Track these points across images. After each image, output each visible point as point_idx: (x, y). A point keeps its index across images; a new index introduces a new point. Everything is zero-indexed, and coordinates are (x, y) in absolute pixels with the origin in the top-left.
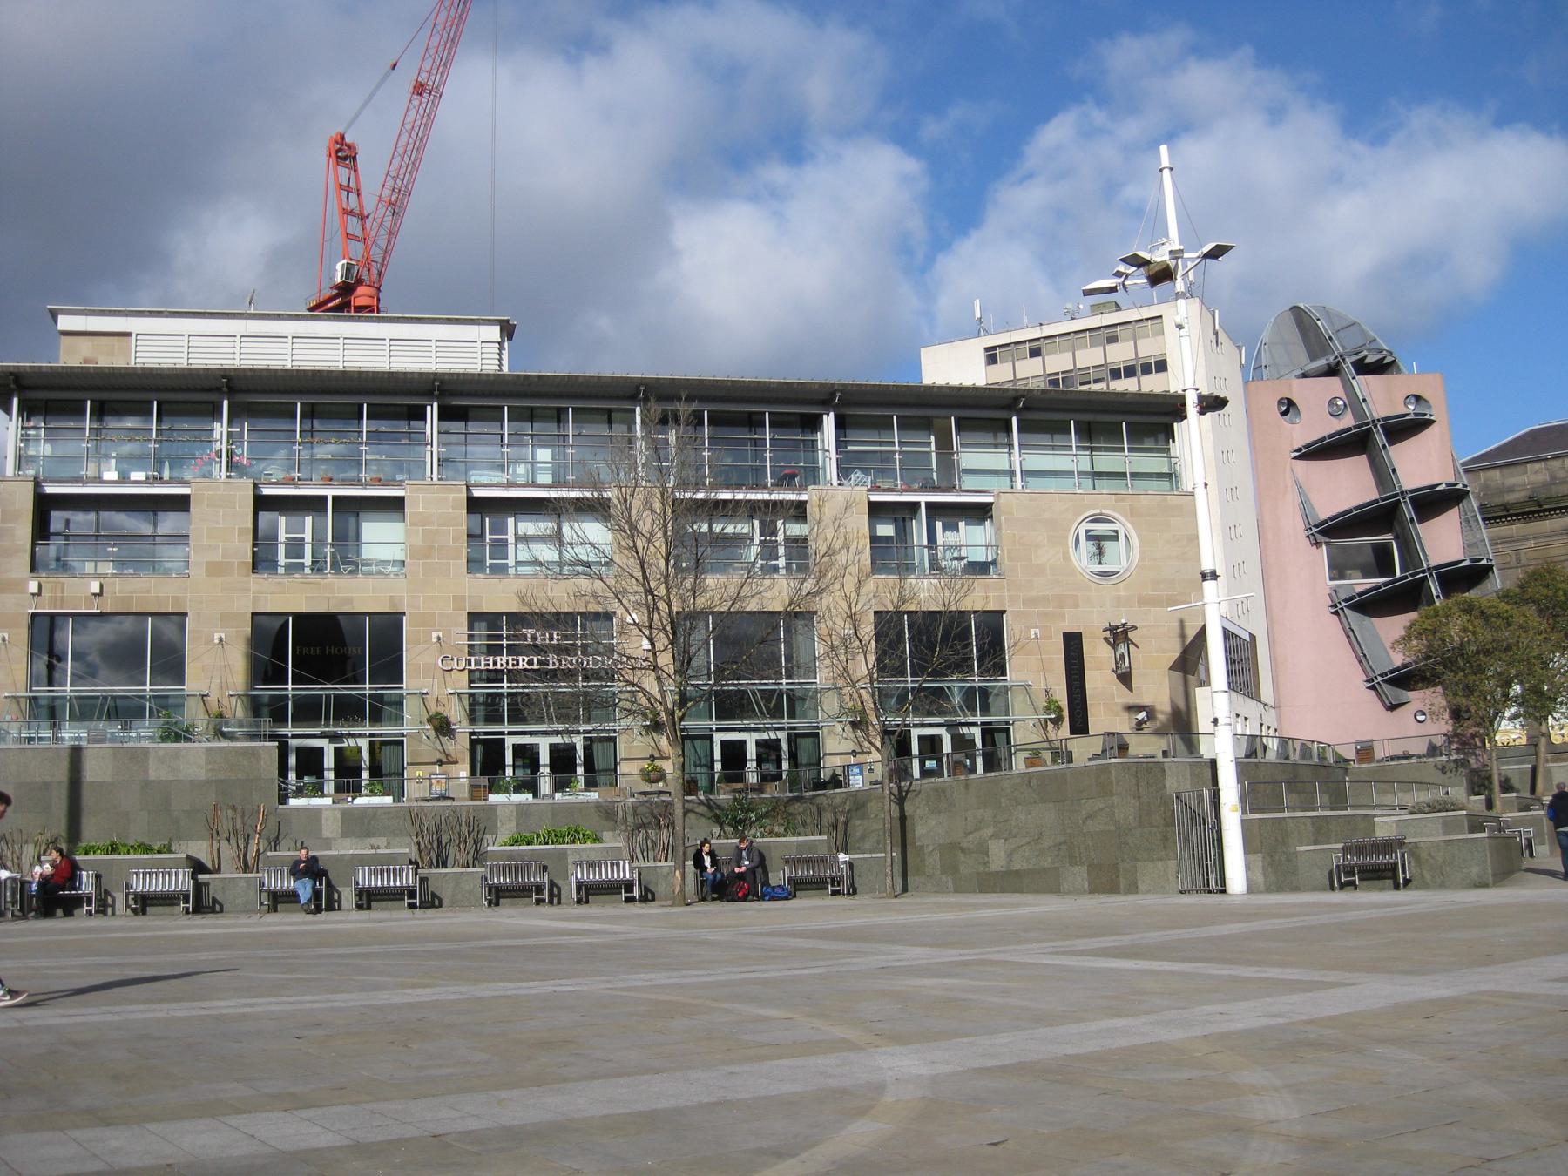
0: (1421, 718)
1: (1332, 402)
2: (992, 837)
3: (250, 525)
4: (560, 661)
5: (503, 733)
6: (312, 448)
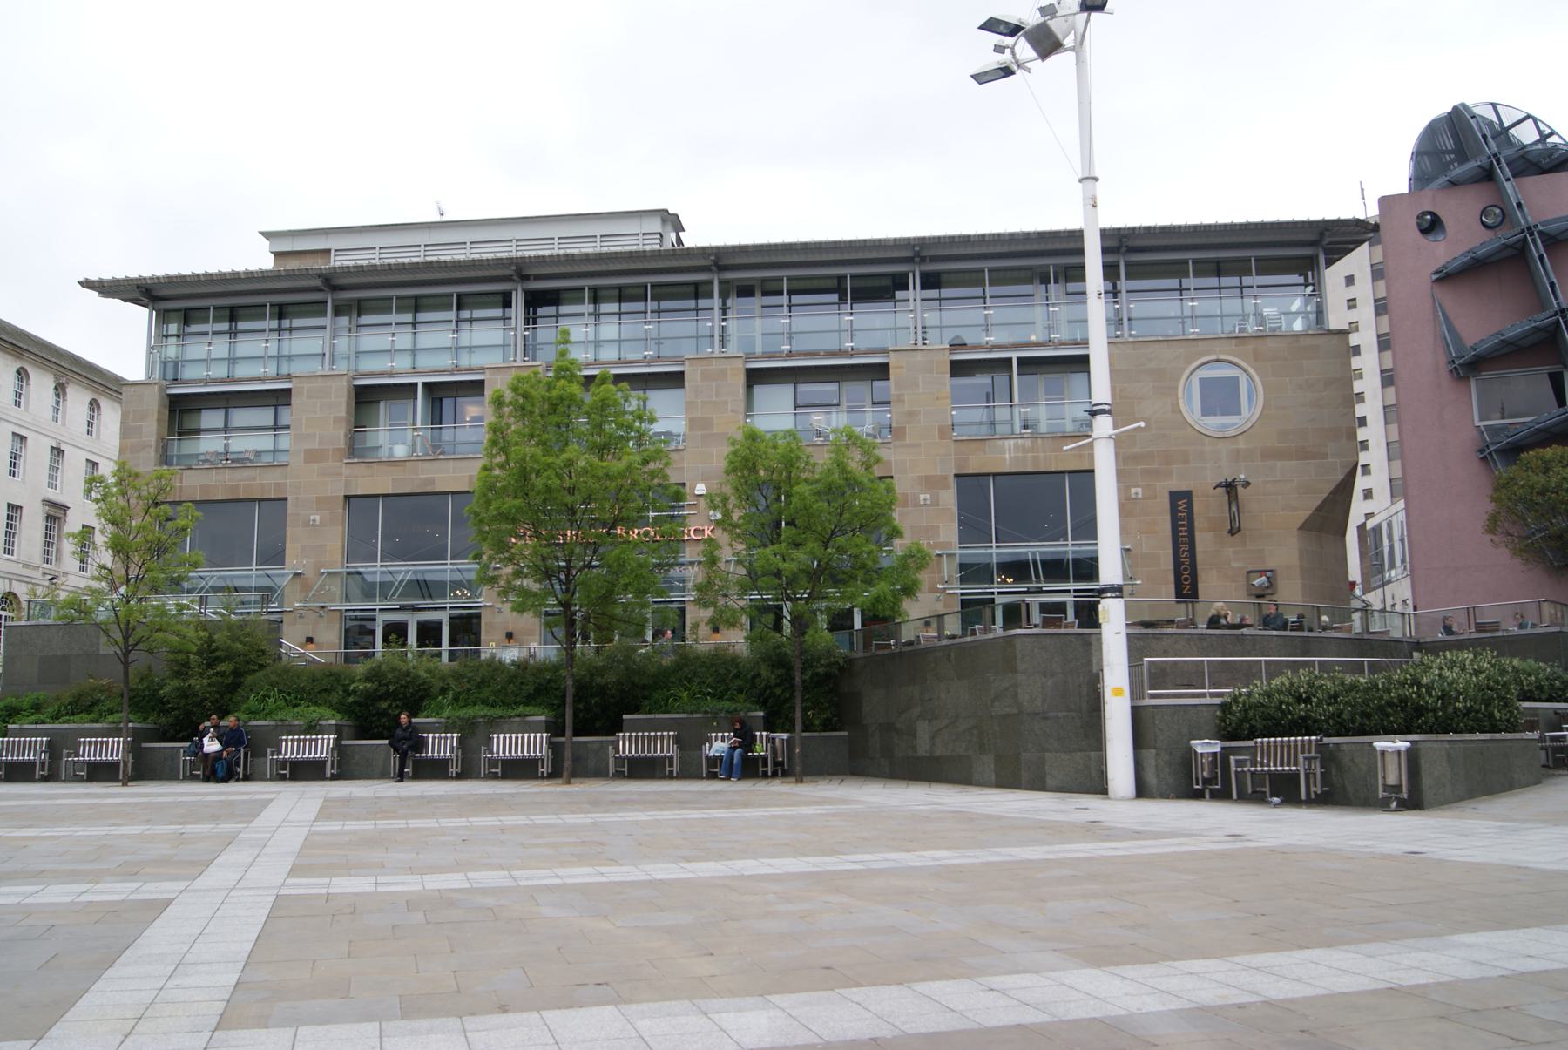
1: (1484, 212)
5: (993, 593)
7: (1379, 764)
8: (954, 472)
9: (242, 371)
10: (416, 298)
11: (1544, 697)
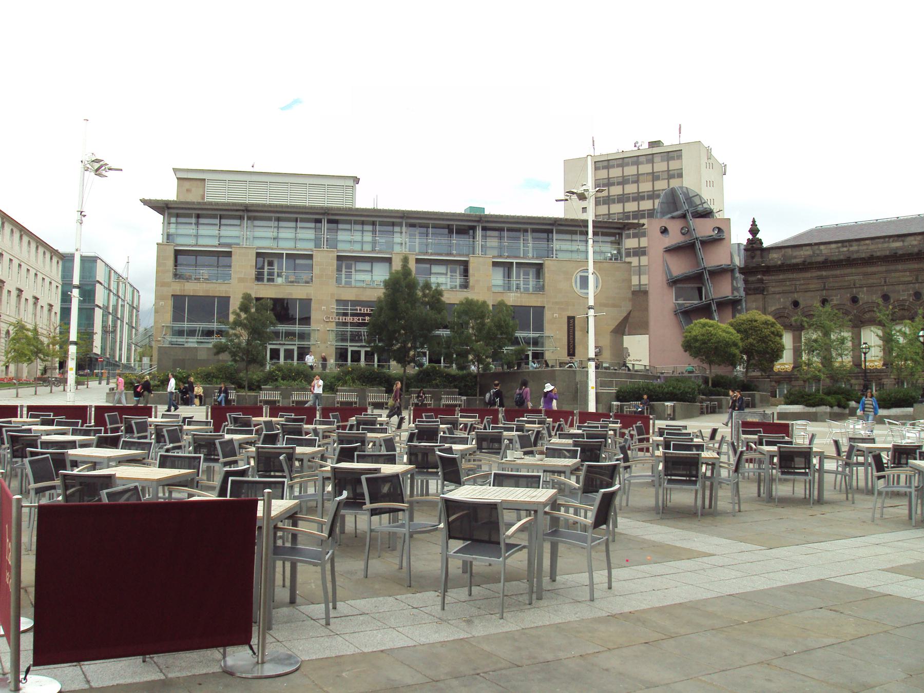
1: (682, 229)
3: (254, 264)
6: (548, 240)
7: (19, 412)
9: (202, 241)
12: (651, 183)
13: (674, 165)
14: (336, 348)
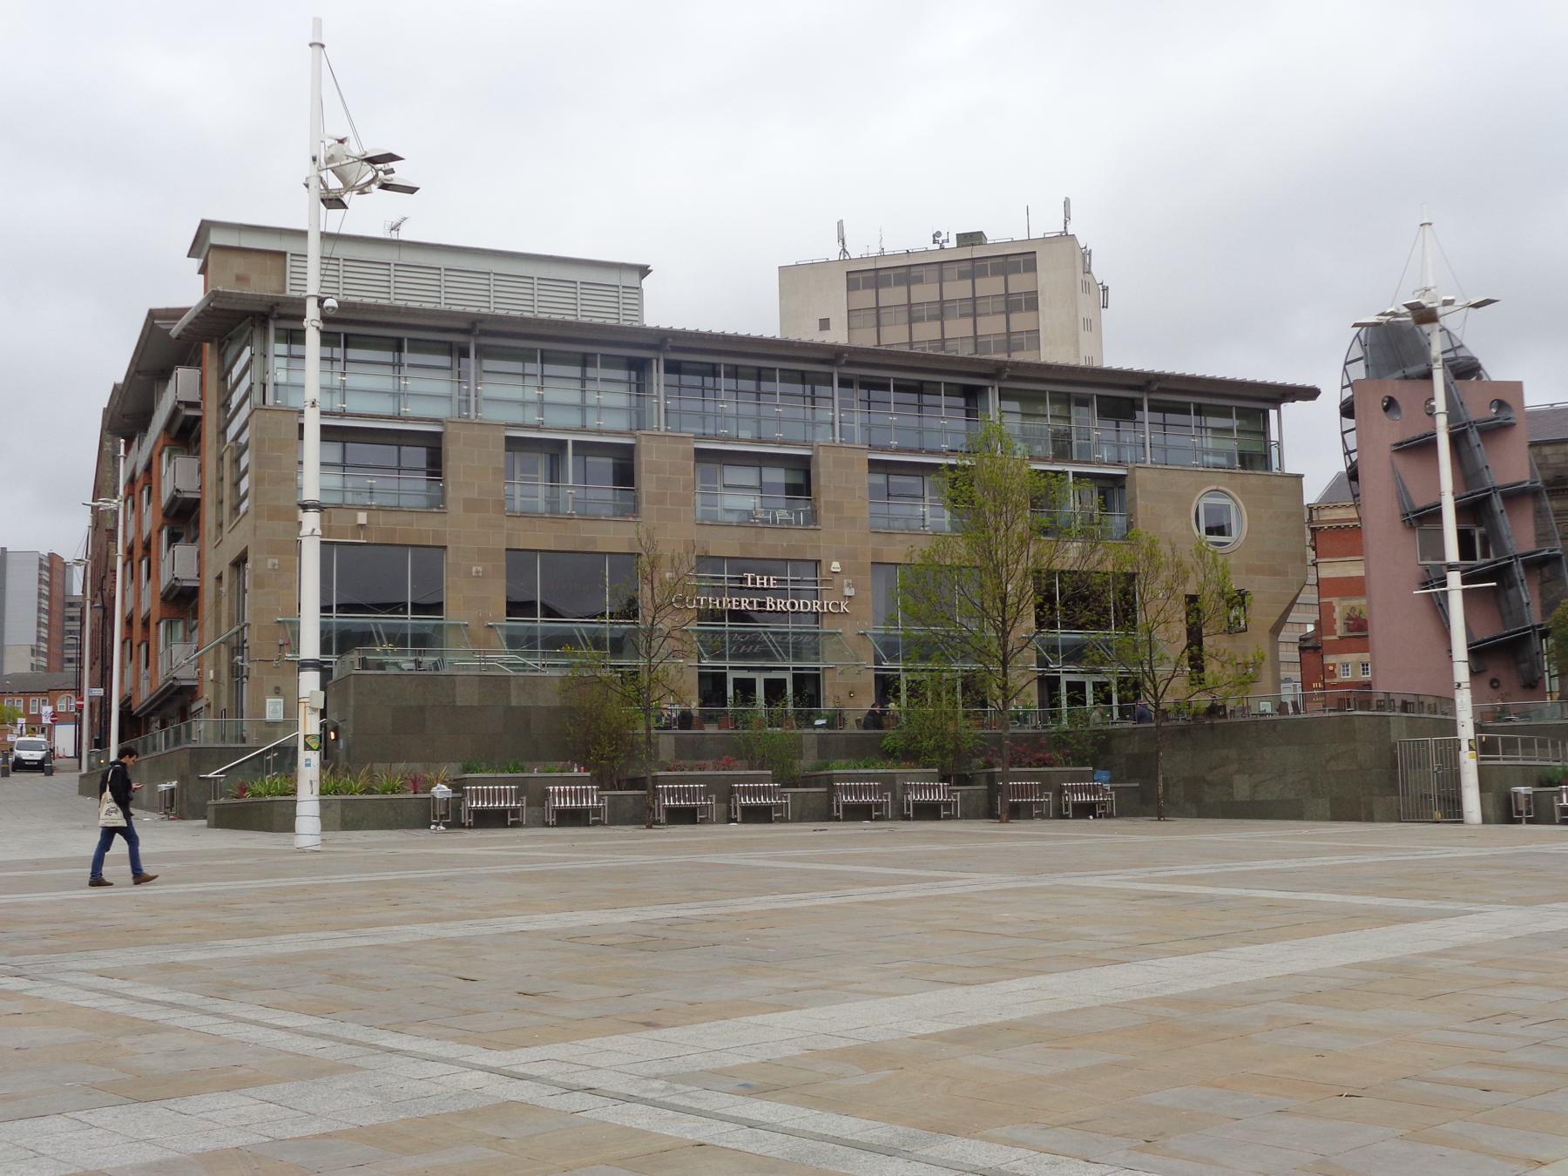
0: (1495, 684)
2: (1238, 772)
4: (775, 604)
5: (725, 668)
8: (505, 547)
10: (760, 369)
11: (557, 769)
12: (906, 328)
13: (1019, 283)
14: (701, 676)
